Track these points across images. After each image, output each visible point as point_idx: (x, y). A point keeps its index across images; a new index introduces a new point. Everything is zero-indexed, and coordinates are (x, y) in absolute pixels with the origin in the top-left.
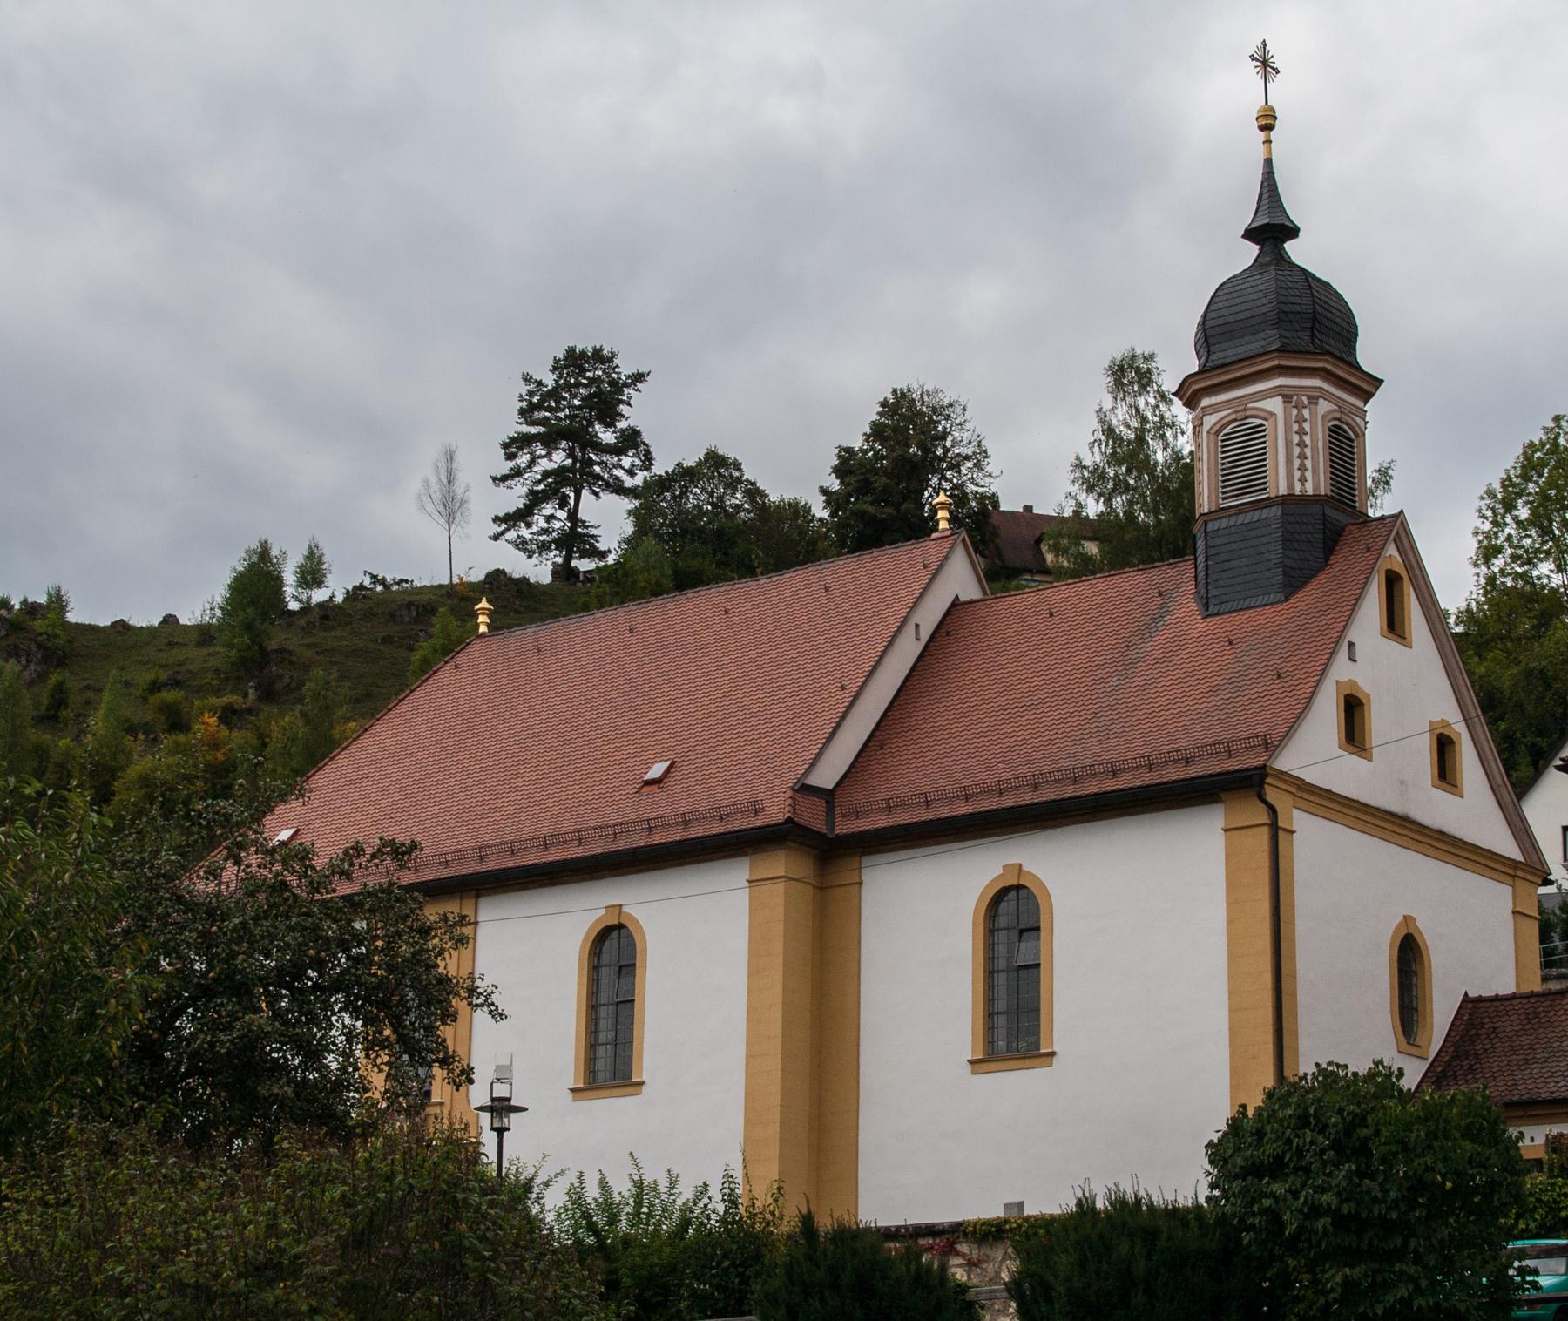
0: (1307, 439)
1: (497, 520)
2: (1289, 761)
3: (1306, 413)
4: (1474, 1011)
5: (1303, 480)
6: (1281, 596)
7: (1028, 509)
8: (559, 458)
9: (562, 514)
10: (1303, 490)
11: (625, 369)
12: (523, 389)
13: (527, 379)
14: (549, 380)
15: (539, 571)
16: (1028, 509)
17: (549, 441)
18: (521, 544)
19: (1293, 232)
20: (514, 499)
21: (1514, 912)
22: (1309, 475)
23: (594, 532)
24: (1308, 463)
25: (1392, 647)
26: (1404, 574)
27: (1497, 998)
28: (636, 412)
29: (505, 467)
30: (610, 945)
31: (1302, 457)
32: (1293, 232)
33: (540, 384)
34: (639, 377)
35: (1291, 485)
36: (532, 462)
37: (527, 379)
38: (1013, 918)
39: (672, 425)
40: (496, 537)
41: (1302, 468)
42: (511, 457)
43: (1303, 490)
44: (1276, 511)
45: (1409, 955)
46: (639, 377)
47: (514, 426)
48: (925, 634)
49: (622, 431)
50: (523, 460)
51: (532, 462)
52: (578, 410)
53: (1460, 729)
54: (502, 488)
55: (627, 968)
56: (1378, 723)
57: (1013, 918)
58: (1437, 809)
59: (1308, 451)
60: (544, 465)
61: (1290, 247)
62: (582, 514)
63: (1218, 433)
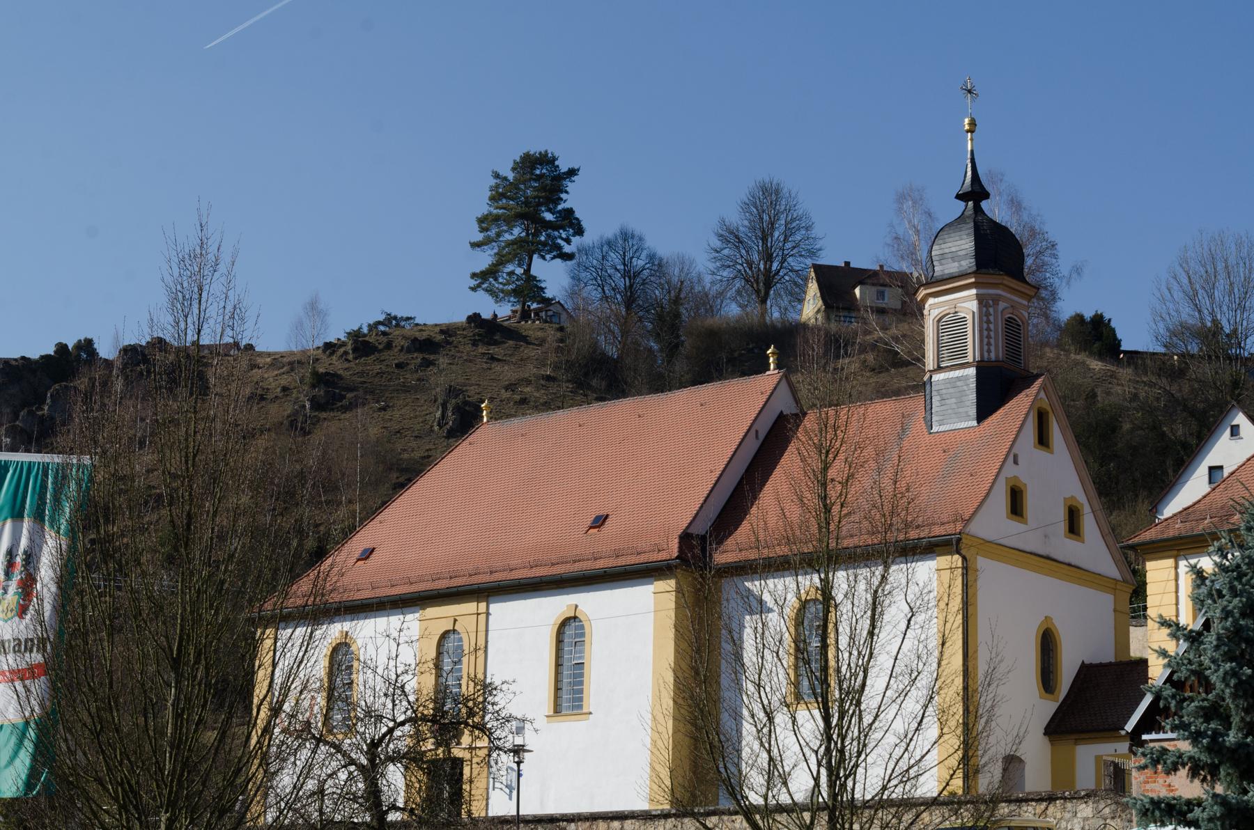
0: (992, 326)
1: (474, 275)
2: (976, 528)
3: (991, 310)
4: (1087, 672)
5: (989, 351)
6: (975, 423)
7: (847, 264)
8: (517, 232)
9: (519, 271)
10: (989, 358)
11: (564, 167)
12: (493, 182)
13: (497, 176)
14: (511, 176)
15: (504, 310)
16: (847, 264)
17: (509, 221)
18: (490, 291)
19: (986, 195)
20: (484, 259)
21: (1115, 610)
22: (992, 348)
23: (543, 285)
24: (992, 341)
25: (1041, 454)
26: (1049, 409)
27: (1101, 665)
28: (574, 197)
29: (479, 237)
30: (569, 631)
31: (989, 337)
32: (986, 195)
33: (505, 179)
34: (572, 172)
35: (982, 355)
36: (499, 235)
37: (497, 176)
38: (569, 632)
39: (596, 206)
40: (474, 289)
41: (989, 344)
42: (483, 230)
43: (989, 358)
44: (972, 371)
45: (1048, 644)
46: (572, 172)
47: (484, 208)
48: (762, 436)
49: (560, 212)
50: (492, 233)
51: (499, 235)
52: (534, 201)
53: (1082, 498)
54: (478, 252)
55: (580, 641)
56: (1031, 503)
57: (569, 632)
58: (1067, 549)
59: (992, 334)
60: (508, 237)
61: (984, 205)
62: (533, 272)
63: (939, 321)
